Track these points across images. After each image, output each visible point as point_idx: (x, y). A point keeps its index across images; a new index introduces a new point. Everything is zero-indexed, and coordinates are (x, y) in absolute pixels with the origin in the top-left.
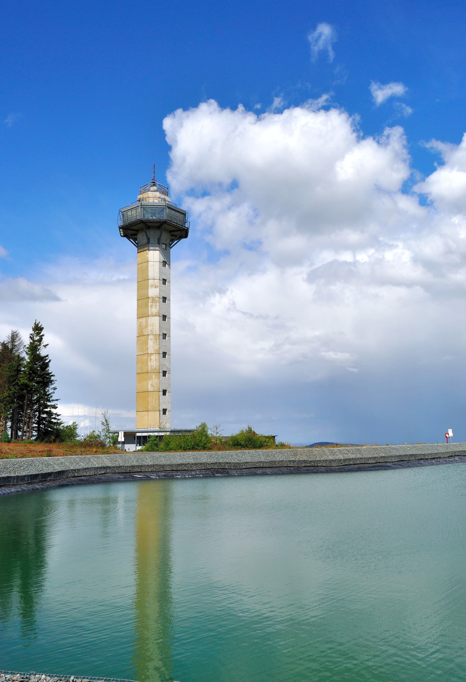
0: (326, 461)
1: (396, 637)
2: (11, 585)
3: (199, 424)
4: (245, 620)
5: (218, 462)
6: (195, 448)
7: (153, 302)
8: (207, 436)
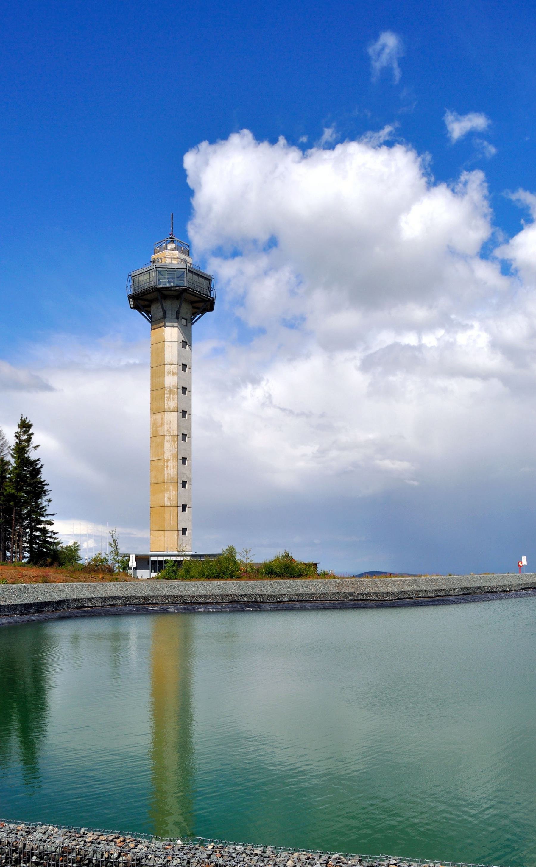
0: (377, 593)
1: (447, 793)
2: (8, 728)
3: (225, 548)
4: (276, 774)
5: (248, 593)
6: (220, 577)
7: (170, 394)
8: (235, 562)
